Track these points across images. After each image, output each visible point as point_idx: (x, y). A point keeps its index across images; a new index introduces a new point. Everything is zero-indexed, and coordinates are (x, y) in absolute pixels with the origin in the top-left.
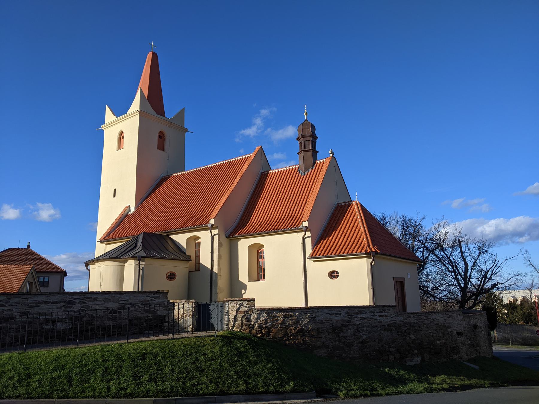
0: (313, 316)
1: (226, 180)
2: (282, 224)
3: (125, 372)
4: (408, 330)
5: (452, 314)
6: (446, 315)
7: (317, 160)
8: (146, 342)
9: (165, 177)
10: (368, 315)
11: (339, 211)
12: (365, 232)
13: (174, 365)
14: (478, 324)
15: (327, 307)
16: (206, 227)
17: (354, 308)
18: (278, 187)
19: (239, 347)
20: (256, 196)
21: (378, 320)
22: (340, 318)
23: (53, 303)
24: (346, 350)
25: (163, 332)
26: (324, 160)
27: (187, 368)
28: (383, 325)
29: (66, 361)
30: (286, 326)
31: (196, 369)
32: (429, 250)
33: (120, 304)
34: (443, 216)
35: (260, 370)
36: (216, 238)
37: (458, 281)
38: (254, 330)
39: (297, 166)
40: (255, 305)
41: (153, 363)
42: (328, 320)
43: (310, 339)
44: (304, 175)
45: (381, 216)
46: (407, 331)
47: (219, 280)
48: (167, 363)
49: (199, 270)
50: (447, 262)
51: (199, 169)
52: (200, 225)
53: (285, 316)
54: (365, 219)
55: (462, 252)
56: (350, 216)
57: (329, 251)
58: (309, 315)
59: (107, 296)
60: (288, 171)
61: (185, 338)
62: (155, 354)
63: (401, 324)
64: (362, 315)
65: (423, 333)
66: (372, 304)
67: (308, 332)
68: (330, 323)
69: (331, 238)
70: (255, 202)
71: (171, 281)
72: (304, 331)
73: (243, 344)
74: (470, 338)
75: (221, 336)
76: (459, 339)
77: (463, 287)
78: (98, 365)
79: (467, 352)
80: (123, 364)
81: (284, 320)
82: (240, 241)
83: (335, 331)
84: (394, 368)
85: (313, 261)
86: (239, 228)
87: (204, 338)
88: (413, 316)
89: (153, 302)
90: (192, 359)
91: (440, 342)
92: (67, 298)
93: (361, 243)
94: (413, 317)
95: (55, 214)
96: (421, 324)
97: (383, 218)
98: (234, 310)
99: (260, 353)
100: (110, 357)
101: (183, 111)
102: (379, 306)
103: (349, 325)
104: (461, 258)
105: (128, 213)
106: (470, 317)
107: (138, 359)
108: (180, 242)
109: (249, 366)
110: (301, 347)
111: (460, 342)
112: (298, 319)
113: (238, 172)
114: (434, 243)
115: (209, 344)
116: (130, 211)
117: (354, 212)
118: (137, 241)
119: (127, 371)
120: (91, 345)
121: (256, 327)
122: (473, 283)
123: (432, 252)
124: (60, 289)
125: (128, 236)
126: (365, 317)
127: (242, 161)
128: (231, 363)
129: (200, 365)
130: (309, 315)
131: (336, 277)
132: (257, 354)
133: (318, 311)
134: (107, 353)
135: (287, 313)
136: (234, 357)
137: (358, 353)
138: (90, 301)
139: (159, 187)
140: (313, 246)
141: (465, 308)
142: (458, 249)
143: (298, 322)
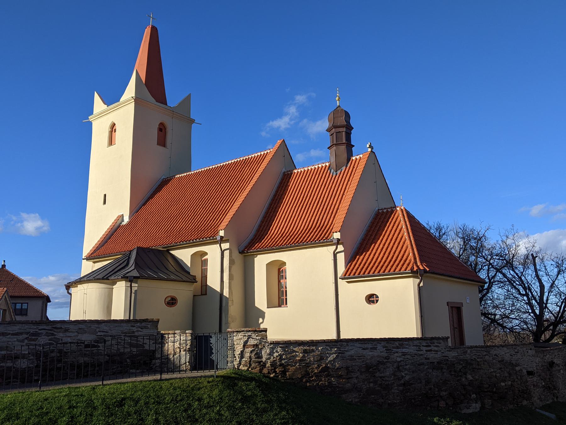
0: (341, 350)
1: (241, 182)
2: (308, 235)
3: (96, 422)
4: (463, 369)
5: (521, 348)
6: (513, 349)
7: (352, 156)
8: (126, 384)
9: (167, 179)
10: (412, 350)
11: (380, 219)
12: (412, 245)
13: (159, 413)
14: (555, 361)
15: (358, 340)
16: (215, 240)
17: (394, 341)
19: (244, 390)
20: (277, 202)
21: (425, 356)
22: (375, 353)
23: (13, 334)
24: (384, 395)
25: (151, 371)
26: (361, 156)
27: (176, 417)
28: (431, 363)
29: (23, 408)
30: (307, 363)
31: (187, 419)
32: (496, 269)
33: (98, 335)
34: (513, 225)
35: (270, 420)
36: (227, 253)
37: (532, 306)
38: (266, 369)
39: (327, 164)
40: (267, 338)
41: (132, 411)
42: (360, 357)
43: (337, 380)
44: (336, 175)
45: (436, 226)
46: (462, 370)
47: (230, 306)
48: (151, 411)
49: (206, 294)
50: (517, 283)
51: (207, 169)
52: (207, 237)
53: (305, 352)
54: (412, 229)
55: (536, 270)
56: (394, 226)
57: (367, 269)
58: (336, 349)
59: (82, 326)
60: (316, 170)
61: (176, 378)
62: (136, 399)
63: (454, 361)
64: (404, 349)
65: (483, 373)
66: (420, 336)
67: (335, 371)
68: (363, 360)
69: (369, 253)
70: (275, 209)
71: (171, 307)
72: (329, 370)
73: (250, 387)
74: (545, 379)
75: (222, 376)
76: (530, 379)
77: (538, 314)
78: (62, 413)
79: (541, 397)
80: (95, 412)
81: (304, 356)
83: (370, 370)
84: (444, 418)
85: (346, 282)
86: (255, 241)
87: (201, 379)
88: (471, 351)
89: (140, 333)
90: (184, 405)
91: (505, 384)
92: (31, 328)
93: (406, 259)
94: (470, 352)
95: (43, 227)
96: (481, 361)
97: (439, 229)
98: (240, 343)
99: (271, 399)
100: (78, 403)
102: (426, 338)
103: (387, 362)
104: (536, 278)
105: (121, 223)
106: (545, 352)
107: (114, 406)
109: (256, 415)
110: (326, 391)
111: (532, 383)
112: (322, 355)
113: (255, 172)
114: (501, 260)
115: (205, 387)
117: (398, 220)
118: (130, 258)
119: (99, 421)
120: (57, 387)
121: (268, 365)
122: (550, 308)
123: (498, 270)
124: (42, 316)
125: (119, 252)
126: (408, 352)
127: (260, 159)
128: (233, 411)
129: (193, 414)
130: (336, 349)
131: (375, 302)
132: (268, 399)
133: (347, 345)
134: (74, 398)
135: (308, 347)
136: (238, 403)
137: (399, 398)
138: (60, 332)
139: (159, 191)
140: (347, 263)
141: (541, 341)
142: (532, 268)
143: (321, 358)
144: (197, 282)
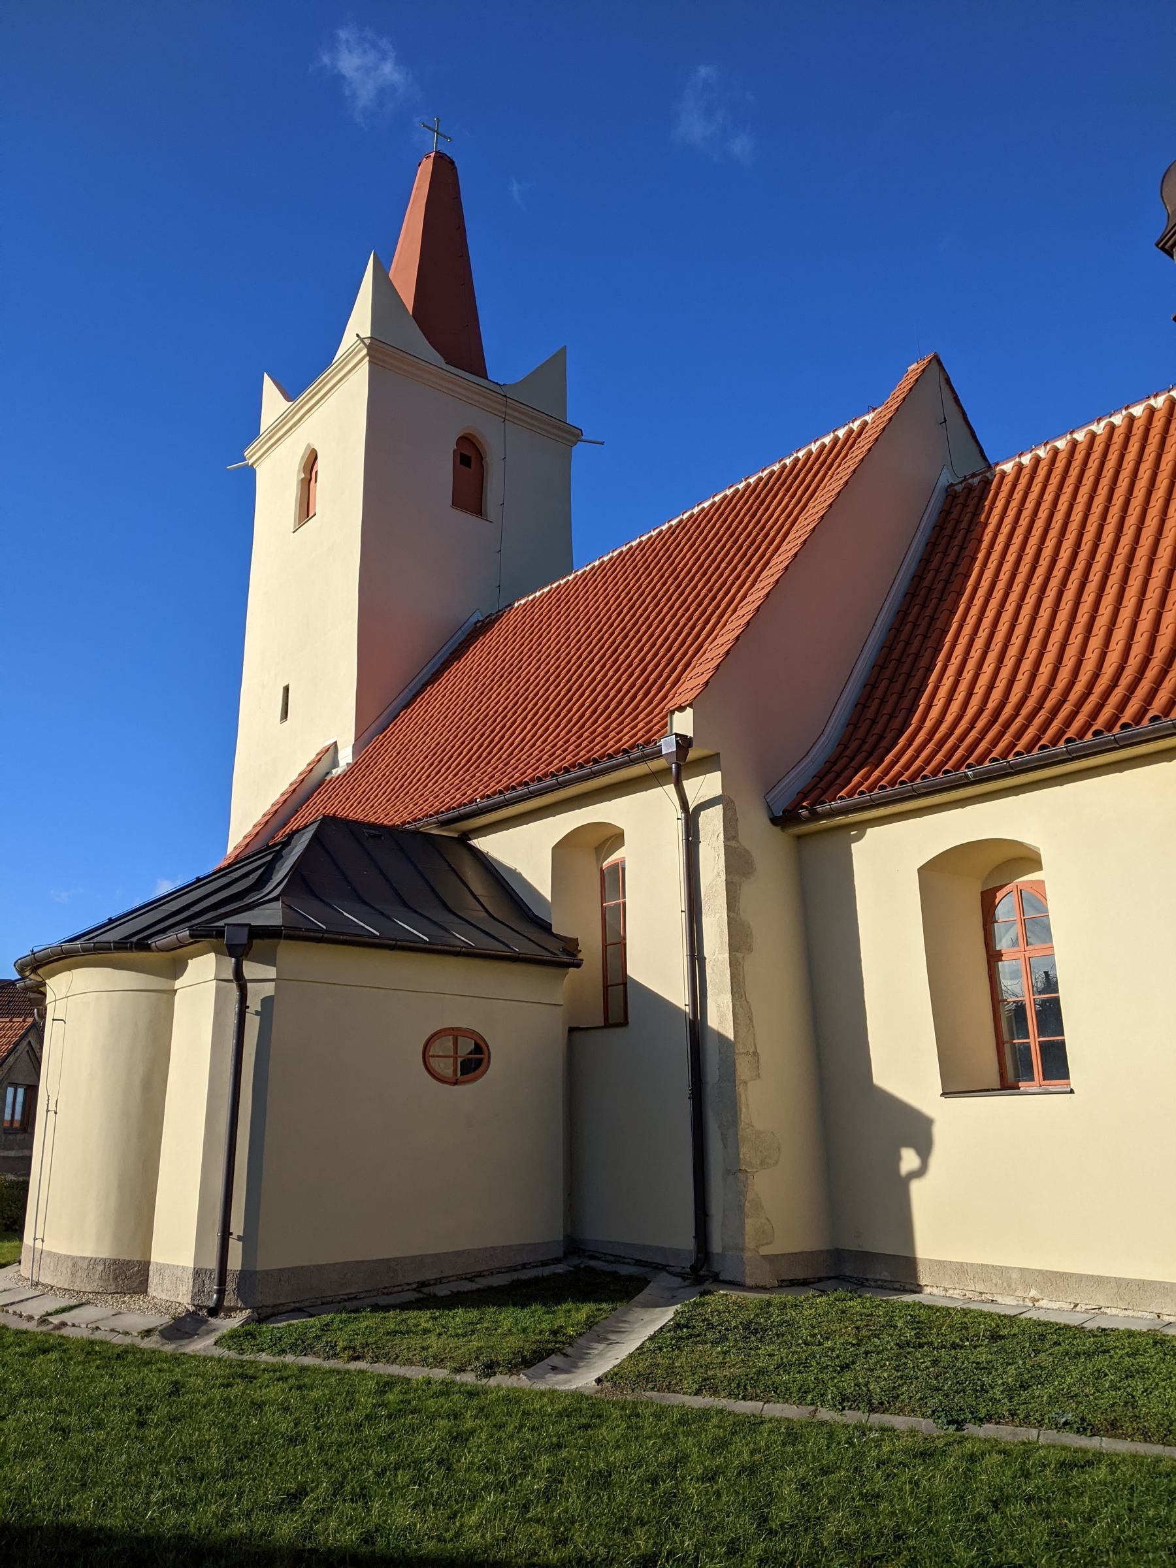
18: (1076, 517)
36: (712, 823)
47: (746, 1083)
82: (859, 838)
101: (559, 360)
108: (519, 870)
116: (338, 766)
139: (459, 658)
144: (578, 966)
